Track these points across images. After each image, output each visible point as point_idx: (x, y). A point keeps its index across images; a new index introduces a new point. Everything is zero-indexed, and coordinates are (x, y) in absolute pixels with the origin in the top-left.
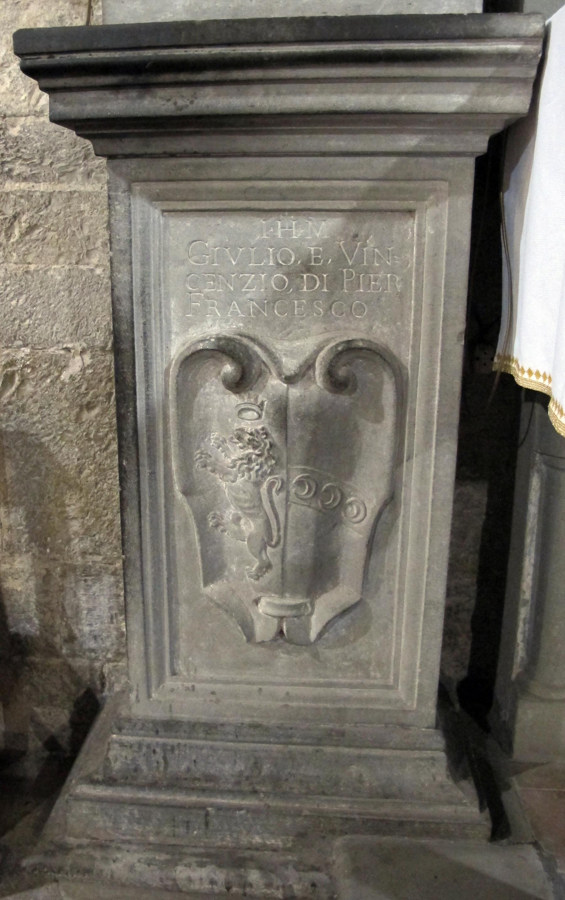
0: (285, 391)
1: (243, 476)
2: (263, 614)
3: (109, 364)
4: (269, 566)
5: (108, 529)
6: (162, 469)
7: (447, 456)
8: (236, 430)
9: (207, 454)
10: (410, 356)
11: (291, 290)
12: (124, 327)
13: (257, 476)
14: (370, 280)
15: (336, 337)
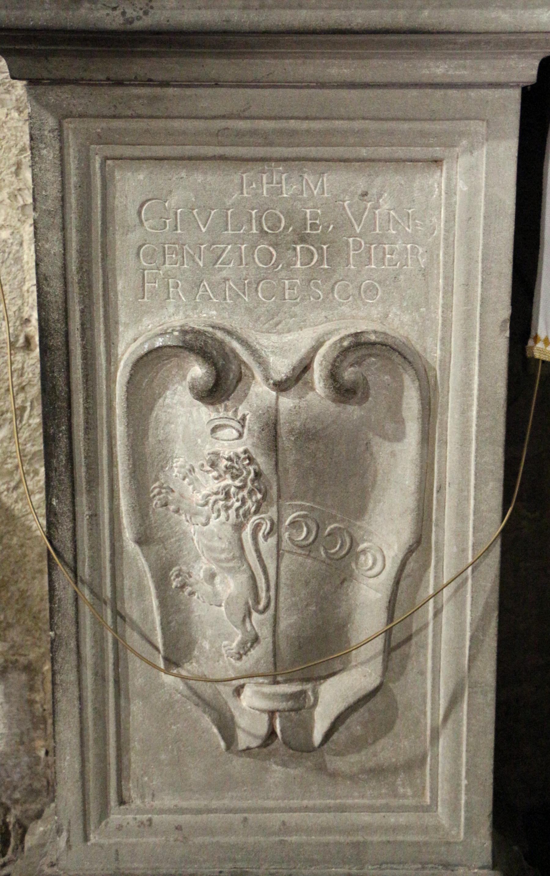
0: (274, 401)
1: (218, 516)
2: (248, 709)
3: (20, 366)
4: (256, 640)
5: (17, 604)
6: (106, 510)
7: (491, 484)
8: (209, 454)
9: (169, 488)
10: (439, 352)
11: (280, 266)
12: (55, 316)
13: (237, 516)
14: (384, 253)
15: (340, 329)
